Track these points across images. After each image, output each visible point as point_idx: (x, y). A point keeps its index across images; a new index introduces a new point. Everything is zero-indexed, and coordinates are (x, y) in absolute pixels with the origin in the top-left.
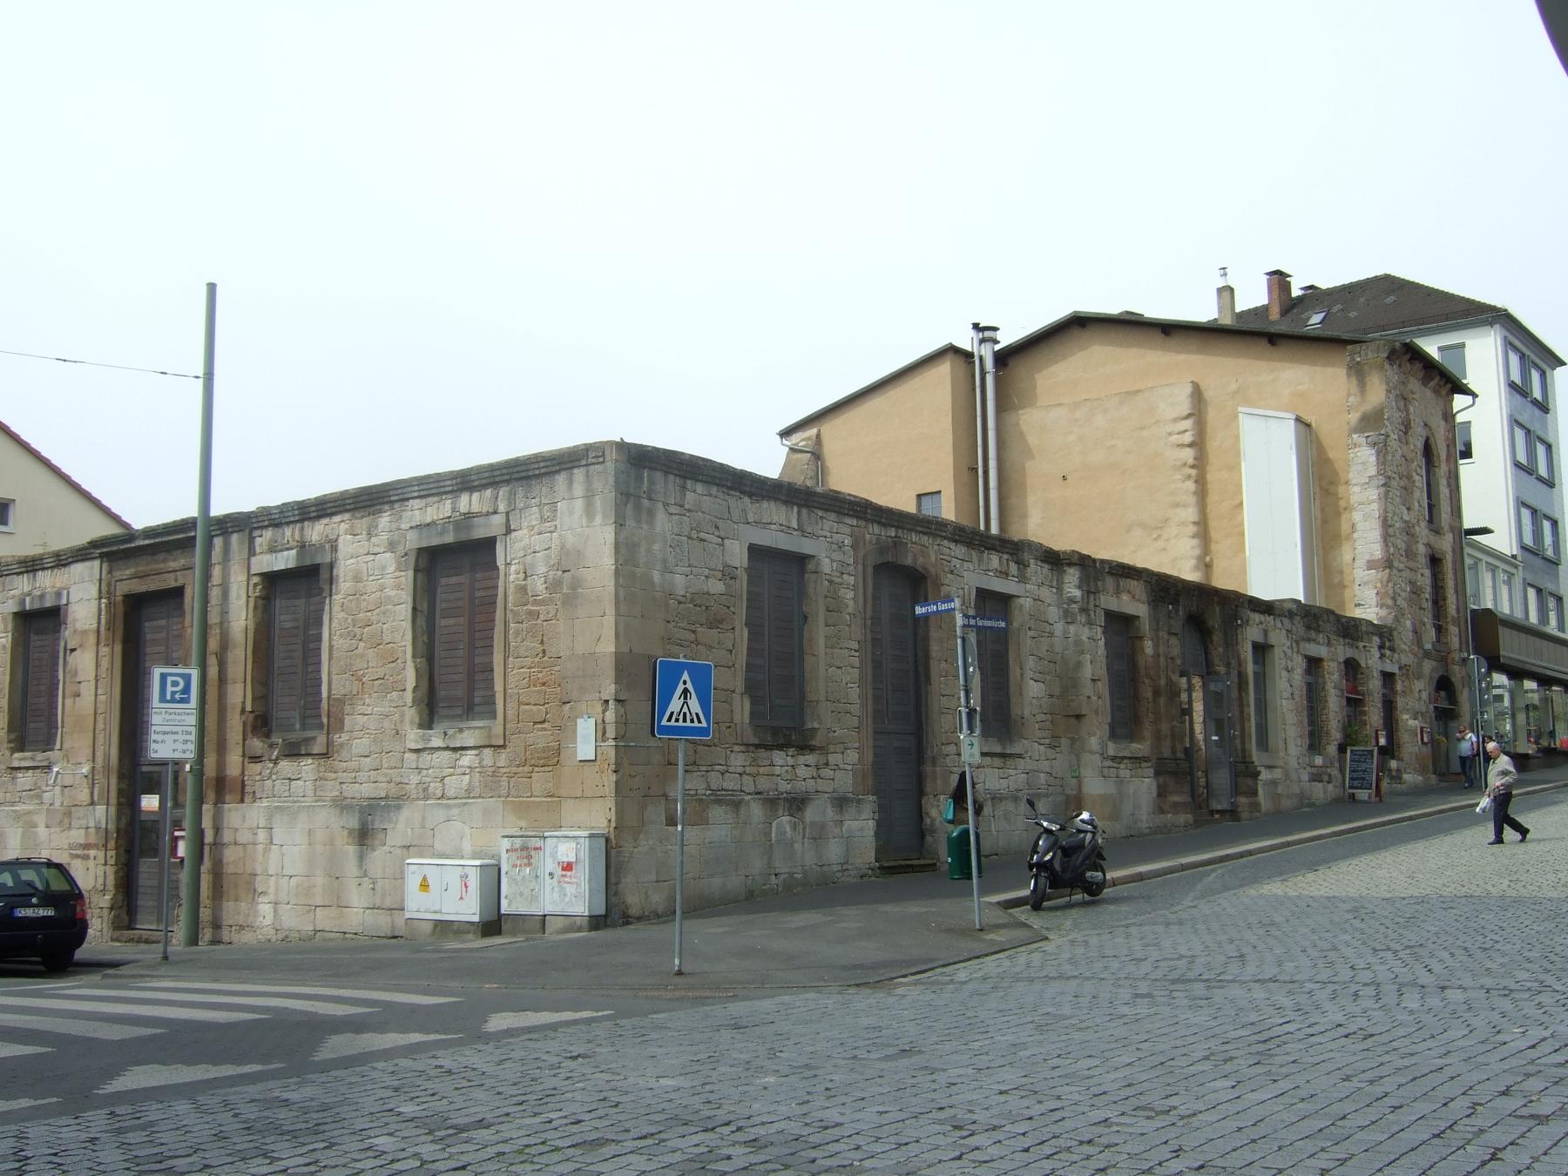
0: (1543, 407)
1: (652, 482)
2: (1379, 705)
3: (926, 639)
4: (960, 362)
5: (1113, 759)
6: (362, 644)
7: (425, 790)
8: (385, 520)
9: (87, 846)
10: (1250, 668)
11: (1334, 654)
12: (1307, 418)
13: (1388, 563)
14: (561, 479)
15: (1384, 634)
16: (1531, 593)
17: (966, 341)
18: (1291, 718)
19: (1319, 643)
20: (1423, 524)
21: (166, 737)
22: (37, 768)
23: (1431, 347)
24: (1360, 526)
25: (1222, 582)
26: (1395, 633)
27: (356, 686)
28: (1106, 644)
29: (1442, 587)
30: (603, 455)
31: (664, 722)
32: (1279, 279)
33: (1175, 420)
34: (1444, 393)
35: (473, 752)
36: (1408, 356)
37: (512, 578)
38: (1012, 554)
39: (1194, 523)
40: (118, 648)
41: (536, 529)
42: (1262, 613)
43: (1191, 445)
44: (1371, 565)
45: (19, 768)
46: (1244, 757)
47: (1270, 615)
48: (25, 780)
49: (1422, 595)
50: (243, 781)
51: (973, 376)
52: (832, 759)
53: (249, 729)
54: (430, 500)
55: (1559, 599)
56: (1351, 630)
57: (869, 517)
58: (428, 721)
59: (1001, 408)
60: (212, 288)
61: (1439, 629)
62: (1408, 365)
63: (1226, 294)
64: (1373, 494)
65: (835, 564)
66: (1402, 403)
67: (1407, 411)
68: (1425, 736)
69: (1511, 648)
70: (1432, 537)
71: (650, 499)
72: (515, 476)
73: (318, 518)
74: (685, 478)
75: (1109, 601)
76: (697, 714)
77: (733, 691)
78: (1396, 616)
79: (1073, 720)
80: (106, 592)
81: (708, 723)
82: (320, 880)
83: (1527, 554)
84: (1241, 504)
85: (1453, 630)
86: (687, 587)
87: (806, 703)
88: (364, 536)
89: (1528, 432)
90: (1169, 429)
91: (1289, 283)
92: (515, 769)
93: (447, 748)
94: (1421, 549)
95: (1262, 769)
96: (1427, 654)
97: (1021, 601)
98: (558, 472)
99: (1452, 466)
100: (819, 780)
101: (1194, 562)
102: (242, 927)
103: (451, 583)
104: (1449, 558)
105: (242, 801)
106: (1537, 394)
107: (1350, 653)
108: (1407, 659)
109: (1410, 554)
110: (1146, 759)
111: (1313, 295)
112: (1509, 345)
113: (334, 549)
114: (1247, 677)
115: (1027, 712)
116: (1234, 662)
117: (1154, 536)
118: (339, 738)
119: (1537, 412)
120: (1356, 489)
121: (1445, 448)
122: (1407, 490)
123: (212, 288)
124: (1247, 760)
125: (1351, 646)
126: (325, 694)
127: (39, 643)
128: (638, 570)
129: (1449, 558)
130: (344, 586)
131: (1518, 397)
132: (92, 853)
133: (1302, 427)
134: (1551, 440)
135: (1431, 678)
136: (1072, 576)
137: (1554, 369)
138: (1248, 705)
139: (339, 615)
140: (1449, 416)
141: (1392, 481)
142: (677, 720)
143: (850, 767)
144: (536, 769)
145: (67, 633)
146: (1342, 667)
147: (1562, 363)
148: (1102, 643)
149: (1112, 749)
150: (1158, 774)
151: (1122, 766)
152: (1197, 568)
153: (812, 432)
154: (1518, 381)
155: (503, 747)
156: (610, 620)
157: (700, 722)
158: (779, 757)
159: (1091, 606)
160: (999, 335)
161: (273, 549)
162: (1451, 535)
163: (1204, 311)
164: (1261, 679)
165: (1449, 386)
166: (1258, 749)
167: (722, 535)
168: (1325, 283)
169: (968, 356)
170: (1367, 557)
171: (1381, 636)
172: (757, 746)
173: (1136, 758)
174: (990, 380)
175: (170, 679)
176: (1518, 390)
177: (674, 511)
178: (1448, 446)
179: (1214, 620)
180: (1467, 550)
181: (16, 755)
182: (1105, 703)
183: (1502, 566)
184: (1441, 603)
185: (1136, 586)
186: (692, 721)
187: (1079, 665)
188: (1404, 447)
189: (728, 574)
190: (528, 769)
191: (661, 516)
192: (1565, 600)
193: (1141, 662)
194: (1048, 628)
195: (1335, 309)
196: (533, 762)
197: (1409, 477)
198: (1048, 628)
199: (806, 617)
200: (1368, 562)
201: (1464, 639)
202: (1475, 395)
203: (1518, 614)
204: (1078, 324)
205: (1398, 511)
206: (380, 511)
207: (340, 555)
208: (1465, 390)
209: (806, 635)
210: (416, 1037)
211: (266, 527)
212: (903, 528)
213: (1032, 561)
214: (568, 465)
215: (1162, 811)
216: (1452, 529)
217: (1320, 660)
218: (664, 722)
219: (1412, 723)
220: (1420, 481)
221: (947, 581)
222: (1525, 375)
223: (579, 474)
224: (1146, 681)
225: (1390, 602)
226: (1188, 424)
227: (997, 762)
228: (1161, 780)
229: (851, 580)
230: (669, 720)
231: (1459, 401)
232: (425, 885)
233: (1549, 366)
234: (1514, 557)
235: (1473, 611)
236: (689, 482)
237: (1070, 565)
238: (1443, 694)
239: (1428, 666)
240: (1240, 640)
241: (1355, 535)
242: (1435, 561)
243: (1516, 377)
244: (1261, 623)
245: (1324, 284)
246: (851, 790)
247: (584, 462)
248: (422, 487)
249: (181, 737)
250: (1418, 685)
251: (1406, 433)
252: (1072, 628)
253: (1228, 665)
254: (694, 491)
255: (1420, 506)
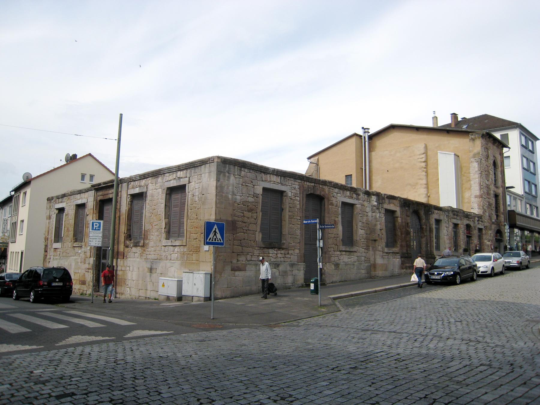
0: (533, 152)
1: (229, 169)
2: (477, 238)
3: (324, 216)
4: (358, 138)
5: (387, 253)
6: (153, 215)
7: (167, 257)
8: (160, 179)
9: (89, 269)
10: (434, 226)
11: (462, 223)
12: (458, 154)
13: (481, 196)
14: (203, 167)
15: (480, 217)
16: (528, 206)
17: (361, 132)
18: (447, 241)
19: (457, 219)
20: (493, 185)
21: (93, 240)
22: (79, 247)
23: (497, 135)
24: (473, 186)
25: (433, 202)
26: (483, 217)
27: (151, 227)
28: (385, 219)
29: (499, 204)
30: (214, 160)
31: (208, 241)
32: (454, 116)
33: (420, 155)
34: (500, 147)
35: (178, 247)
36: (488, 136)
37: (190, 196)
38: (354, 192)
39: (425, 184)
40: (97, 215)
41: (196, 182)
42: (438, 210)
43: (424, 162)
44: (476, 197)
45: (75, 247)
46: (431, 253)
47: (441, 211)
48: (76, 249)
49: (492, 206)
50: (124, 253)
51: (362, 142)
52: (290, 252)
53: (126, 238)
54: (171, 173)
55: (537, 208)
56: (467, 216)
57: (305, 180)
58: (168, 238)
59: (370, 151)
60: (121, 115)
61: (497, 216)
62: (488, 139)
63: (435, 119)
64: (477, 176)
65: (293, 194)
66: (486, 150)
67: (488, 152)
68: (492, 246)
69: (519, 222)
70: (495, 189)
71: (229, 173)
72: (191, 166)
73: (144, 179)
74: (241, 167)
75: (387, 206)
76: (220, 239)
77: (256, 231)
78: (483, 212)
79: (373, 242)
80: (95, 199)
81: (223, 242)
82: (140, 282)
83: (526, 194)
84: (438, 179)
85: (502, 216)
86: (241, 200)
87: (282, 235)
88: (154, 184)
89: (527, 159)
90: (418, 157)
91: (457, 117)
92: (189, 253)
93: (172, 246)
94: (492, 192)
95: (437, 257)
96: (493, 223)
97: (357, 206)
98: (202, 165)
99: (503, 169)
100: (285, 258)
101: (424, 195)
102: (122, 294)
103: (176, 197)
104: (501, 195)
105: (124, 258)
106: (530, 148)
107: (468, 222)
108: (486, 224)
109: (488, 194)
110: (398, 253)
111: (464, 120)
112: (521, 134)
113: (147, 188)
114: (433, 229)
115: (358, 239)
116: (428, 225)
117: (414, 188)
118: (147, 242)
119: (530, 153)
120: (472, 175)
121: (500, 163)
122: (487, 175)
123: (121, 115)
124: (432, 253)
125: (468, 220)
126: (143, 229)
127: (106, 212)
128: (223, 194)
129: (501, 195)
130: (149, 198)
131: (524, 149)
132: (90, 271)
133: (456, 157)
134: (535, 161)
135: (494, 230)
136: (374, 198)
137: (536, 141)
138: (433, 237)
139: (148, 206)
140: (502, 154)
141: (484, 173)
142: (212, 240)
143: (296, 254)
144: (194, 253)
145: (86, 210)
146: (465, 226)
147: (538, 139)
148: (384, 218)
149: (386, 250)
150: (401, 257)
151: (390, 255)
152: (425, 197)
153: (316, 158)
154: (524, 144)
155: (186, 246)
156: (214, 209)
157: (220, 241)
158: (271, 251)
159: (380, 207)
160: (370, 131)
161: (133, 188)
162: (502, 188)
163: (430, 125)
164: (438, 230)
165: (502, 145)
166: (436, 251)
167: (254, 184)
168: (468, 117)
169: (361, 136)
170: (475, 194)
171: (478, 217)
172: (264, 248)
173: (394, 253)
174: (367, 143)
175: (95, 224)
176: (524, 147)
177: (237, 177)
178: (501, 163)
179: (422, 213)
180: (507, 193)
181: (75, 243)
182: (384, 236)
183: (518, 198)
184: (498, 208)
185: (397, 202)
186: (218, 241)
187: (376, 225)
188: (487, 163)
189: (255, 196)
190: (192, 252)
191: (232, 178)
192: (539, 208)
193: (397, 224)
194: (366, 214)
195: (471, 124)
196: (193, 251)
197: (488, 171)
198: (366, 214)
199: (283, 209)
200: (475, 196)
201: (505, 219)
202: (509, 148)
203: (523, 213)
204: (392, 128)
205: (484, 181)
206: (159, 177)
207: (149, 190)
208: (506, 147)
209: (283, 215)
210: (100, 338)
211: (132, 181)
212: (317, 183)
213: (361, 194)
214: (205, 163)
215: (403, 269)
216: (502, 187)
217: (458, 224)
218: (208, 241)
219: (488, 243)
220: (492, 172)
221: (332, 199)
222: (527, 142)
223: (207, 165)
224: (399, 230)
225: (482, 208)
226: (424, 156)
227: (347, 253)
228: (403, 259)
229: (298, 198)
230: (209, 240)
231: (505, 150)
232: (163, 285)
233: (534, 140)
234: (522, 195)
235: (509, 211)
236: (243, 169)
237: (374, 195)
238: (498, 235)
239: (493, 227)
240: (430, 218)
241: (471, 188)
242: (496, 196)
243: (524, 143)
244: (438, 213)
245: (468, 117)
246: (296, 261)
247: (208, 162)
248: (169, 170)
249: (98, 240)
250: (490, 232)
251: (487, 159)
252: (374, 214)
253: (426, 225)
254: (245, 171)
255: (492, 180)
